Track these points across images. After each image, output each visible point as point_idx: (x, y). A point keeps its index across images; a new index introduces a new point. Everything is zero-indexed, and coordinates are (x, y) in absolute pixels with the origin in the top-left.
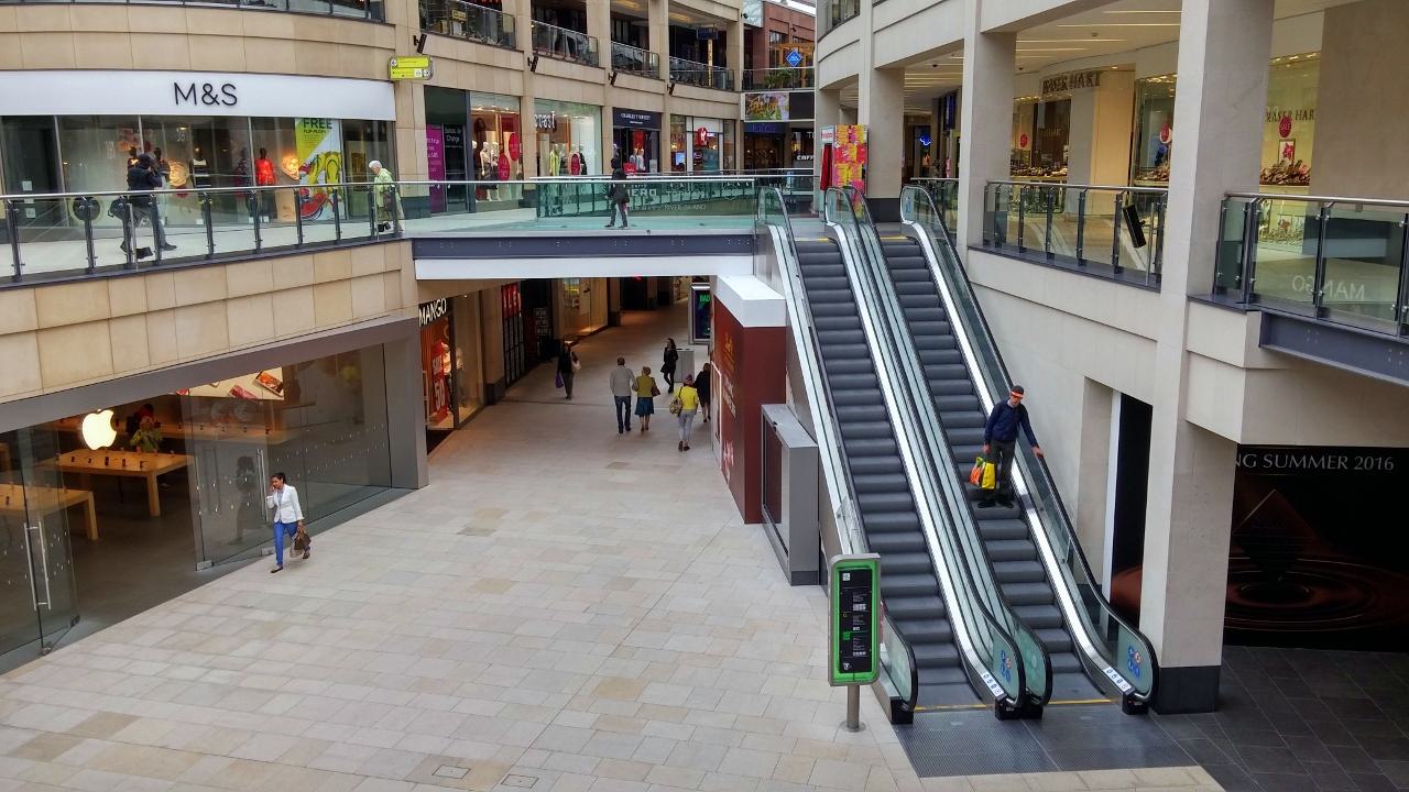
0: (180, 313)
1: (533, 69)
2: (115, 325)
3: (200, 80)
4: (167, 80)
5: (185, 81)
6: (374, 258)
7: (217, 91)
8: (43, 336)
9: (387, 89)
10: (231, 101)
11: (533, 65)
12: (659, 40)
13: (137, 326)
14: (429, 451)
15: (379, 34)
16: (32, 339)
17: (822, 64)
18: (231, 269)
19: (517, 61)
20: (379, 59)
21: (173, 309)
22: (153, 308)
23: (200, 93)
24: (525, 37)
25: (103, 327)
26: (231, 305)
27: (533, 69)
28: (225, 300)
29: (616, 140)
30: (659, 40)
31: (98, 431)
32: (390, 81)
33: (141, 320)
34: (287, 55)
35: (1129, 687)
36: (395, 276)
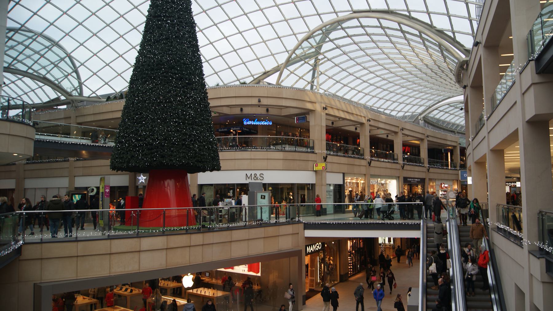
0: (214, 245)
1: (370, 165)
2: (192, 248)
3: (253, 172)
4: (245, 172)
5: (249, 173)
6: (289, 229)
7: (258, 175)
8: (168, 250)
9: (313, 174)
10: (262, 178)
11: (370, 164)
12: (424, 154)
13: (199, 249)
14: (517, 129)
15: (311, 156)
16: (165, 251)
17: (526, 95)
18: (234, 232)
19: (363, 162)
20: (310, 164)
21: (212, 244)
22: (205, 243)
23: (253, 176)
24: (367, 156)
25: (188, 249)
26: (233, 243)
27: (370, 165)
28: (231, 242)
29: (320, 216)
30: (424, 154)
31: (188, 281)
32: (314, 171)
33: (201, 247)
34: (280, 164)
35: (463, 123)
36: (297, 235)
